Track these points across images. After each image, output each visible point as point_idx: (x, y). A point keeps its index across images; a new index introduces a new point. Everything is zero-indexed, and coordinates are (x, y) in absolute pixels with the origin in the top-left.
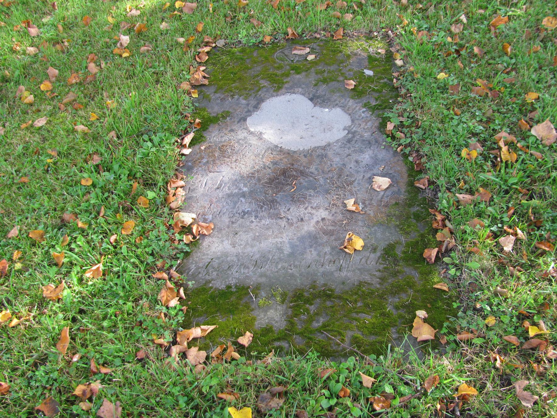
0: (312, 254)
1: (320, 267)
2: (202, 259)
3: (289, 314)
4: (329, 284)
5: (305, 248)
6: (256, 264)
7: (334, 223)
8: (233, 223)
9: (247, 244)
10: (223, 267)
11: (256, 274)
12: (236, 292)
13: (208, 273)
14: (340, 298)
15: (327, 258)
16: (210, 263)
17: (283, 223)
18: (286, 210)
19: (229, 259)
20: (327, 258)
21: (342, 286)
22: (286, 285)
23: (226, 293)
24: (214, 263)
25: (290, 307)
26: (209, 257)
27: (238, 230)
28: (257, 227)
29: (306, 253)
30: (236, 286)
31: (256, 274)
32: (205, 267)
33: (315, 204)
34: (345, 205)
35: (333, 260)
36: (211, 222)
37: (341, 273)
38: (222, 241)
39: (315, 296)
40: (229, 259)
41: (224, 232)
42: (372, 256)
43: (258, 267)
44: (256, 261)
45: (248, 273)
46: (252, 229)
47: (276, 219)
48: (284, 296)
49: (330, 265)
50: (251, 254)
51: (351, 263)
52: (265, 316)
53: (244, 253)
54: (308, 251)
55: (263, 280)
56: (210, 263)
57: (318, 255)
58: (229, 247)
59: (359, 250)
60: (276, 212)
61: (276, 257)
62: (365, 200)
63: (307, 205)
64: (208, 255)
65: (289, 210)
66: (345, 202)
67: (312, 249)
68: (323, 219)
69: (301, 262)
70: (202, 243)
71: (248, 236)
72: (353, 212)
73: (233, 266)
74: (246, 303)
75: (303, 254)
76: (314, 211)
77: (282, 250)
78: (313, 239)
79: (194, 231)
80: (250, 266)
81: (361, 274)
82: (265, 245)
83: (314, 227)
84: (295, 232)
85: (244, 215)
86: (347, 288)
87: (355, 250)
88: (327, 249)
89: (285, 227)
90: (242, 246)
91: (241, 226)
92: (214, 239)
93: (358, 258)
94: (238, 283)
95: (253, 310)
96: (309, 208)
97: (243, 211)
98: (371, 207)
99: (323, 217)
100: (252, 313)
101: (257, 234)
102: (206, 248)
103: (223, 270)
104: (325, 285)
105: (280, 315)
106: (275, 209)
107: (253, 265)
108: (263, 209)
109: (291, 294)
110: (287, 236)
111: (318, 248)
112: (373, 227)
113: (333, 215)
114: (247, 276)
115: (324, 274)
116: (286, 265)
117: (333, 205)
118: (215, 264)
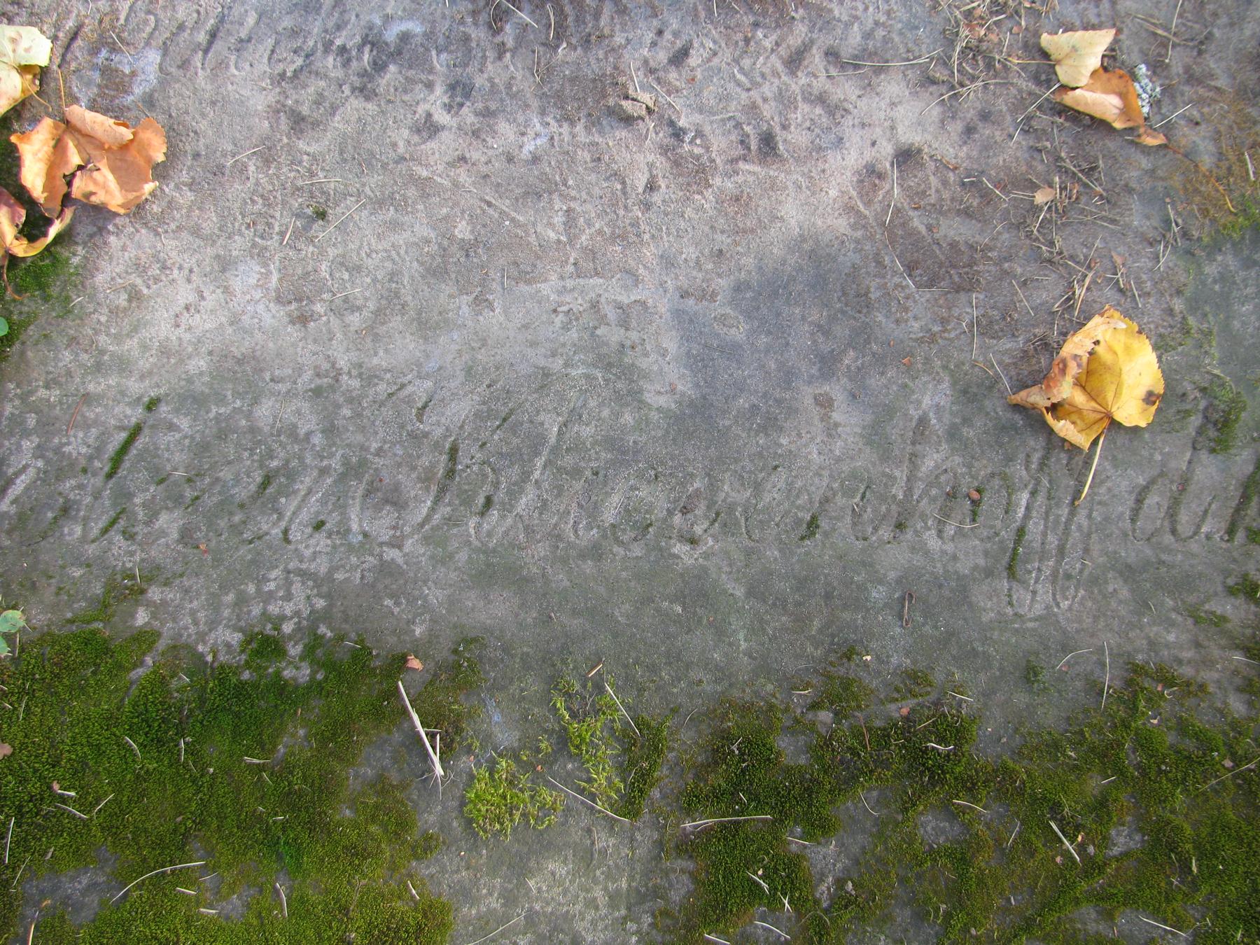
0: (831, 430)
1: (885, 533)
2: (87, 399)
3: (676, 896)
4: (938, 677)
5: (788, 377)
6: (450, 473)
7: (976, 194)
8: (298, 122)
9: (390, 302)
10: (226, 474)
11: (445, 560)
12: (315, 688)
13: (120, 518)
14: (1001, 782)
15: (930, 462)
16: (136, 432)
17: (640, 157)
18: (662, 56)
19: (265, 411)
20: (930, 462)
21: (1021, 699)
22: (653, 669)
23: (239, 697)
24: (166, 439)
25: (685, 847)
26: (134, 386)
27: (333, 183)
28: (463, 176)
29: (792, 411)
30: (314, 645)
31: (445, 560)
32: (101, 465)
33: (855, 37)
34: (1044, 66)
35: (967, 485)
36: (149, 101)
37: (1021, 594)
38: (225, 264)
39: (841, 765)
40: (265, 411)
41: (236, 190)
42: (1208, 470)
43: (467, 501)
44: (454, 451)
45: (397, 544)
46: (425, 187)
47: (593, 122)
48: (640, 748)
49: (950, 530)
50: (420, 390)
51: (1081, 518)
52: (510, 899)
53: (370, 378)
54: (806, 395)
55: (494, 611)
56: (136, 432)
57: (875, 436)
58: (271, 315)
59: (1136, 429)
60: (595, 63)
61: (587, 431)
62: (1164, 44)
63: (800, 32)
64: (123, 365)
65: (678, 59)
66: (1046, 40)
67: (836, 391)
68: (906, 157)
69: (758, 487)
70: (88, 269)
71: (401, 238)
72: (1099, 125)
73: (292, 476)
74: (381, 786)
75: (770, 425)
76: (846, 89)
77: (629, 373)
78: (826, 294)
79: (33, 176)
80: (410, 486)
81: (1143, 605)
82: (517, 324)
83: (849, 209)
84: (723, 240)
85: (379, 67)
86: (1050, 716)
87: (1114, 425)
88: (933, 398)
89: (651, 187)
90: (355, 320)
91: (355, 154)
92: (170, 246)
93: (1125, 482)
94: (324, 616)
95: (425, 847)
96: (816, 59)
97: (371, 40)
98: (1200, 102)
99: (909, 136)
100: (425, 869)
101: (462, 230)
102: (114, 312)
103: (225, 505)
104: (915, 679)
105: (614, 898)
106: (586, 42)
107: (426, 479)
108: (509, 34)
109: (685, 742)
110: (668, 262)
111: (875, 381)
112: (1210, 258)
113: (969, 130)
114: (386, 569)
115: (907, 598)
116: (656, 498)
117: (974, 51)
118: (172, 445)
